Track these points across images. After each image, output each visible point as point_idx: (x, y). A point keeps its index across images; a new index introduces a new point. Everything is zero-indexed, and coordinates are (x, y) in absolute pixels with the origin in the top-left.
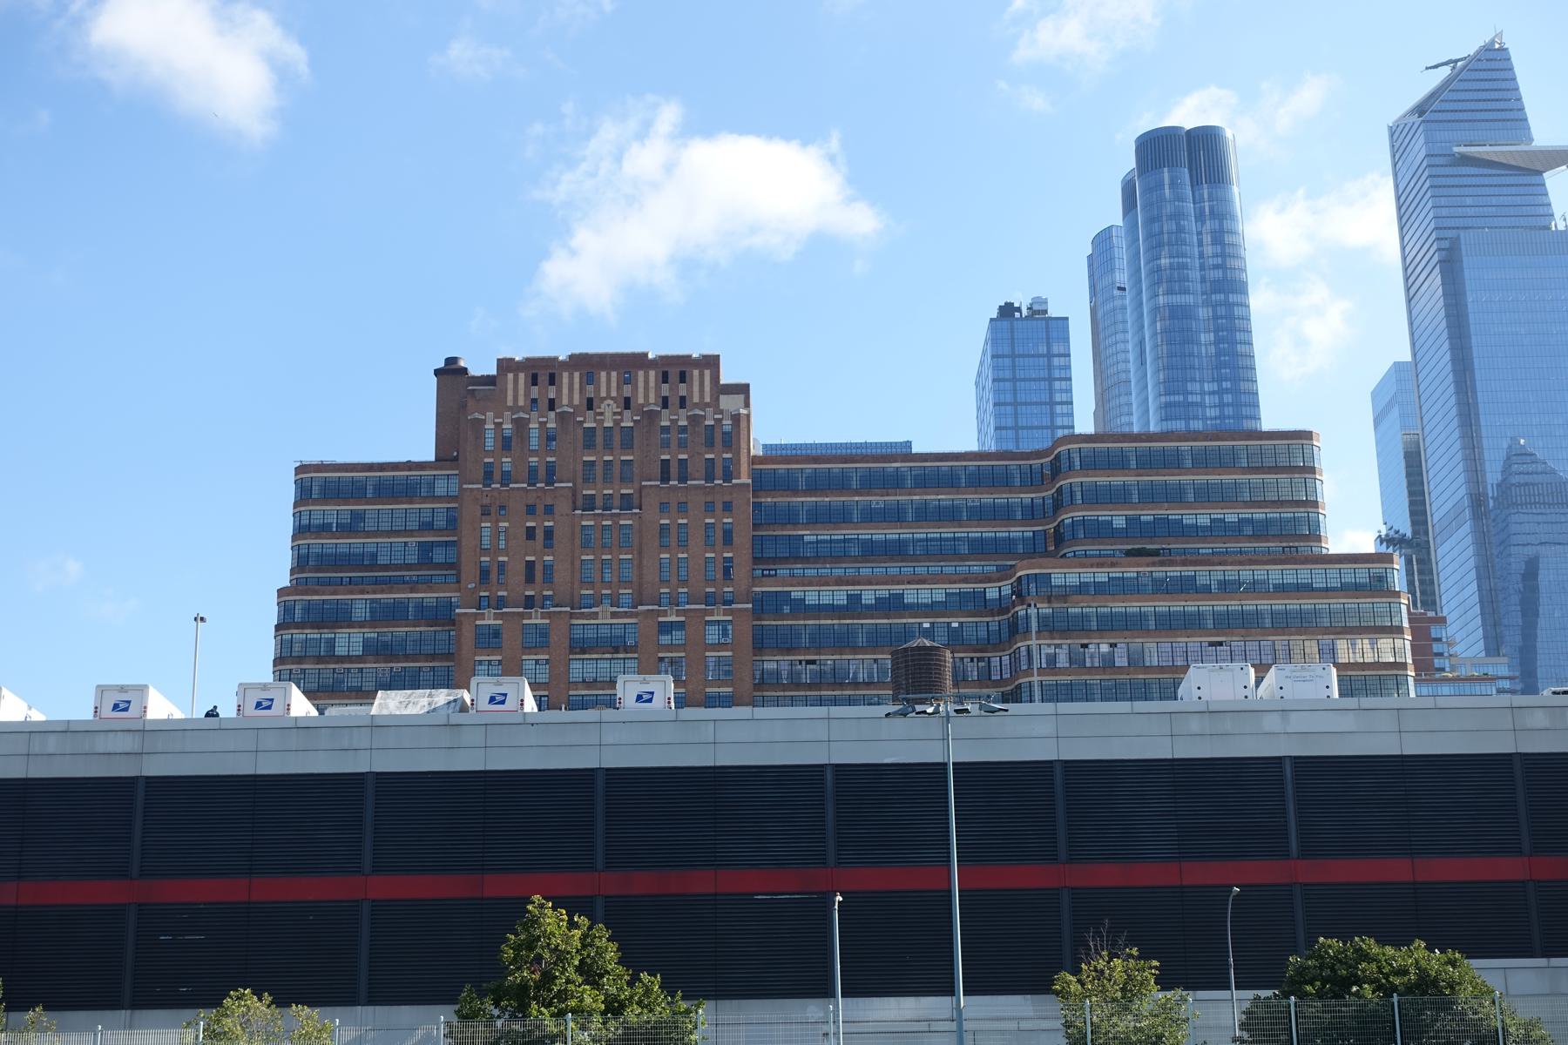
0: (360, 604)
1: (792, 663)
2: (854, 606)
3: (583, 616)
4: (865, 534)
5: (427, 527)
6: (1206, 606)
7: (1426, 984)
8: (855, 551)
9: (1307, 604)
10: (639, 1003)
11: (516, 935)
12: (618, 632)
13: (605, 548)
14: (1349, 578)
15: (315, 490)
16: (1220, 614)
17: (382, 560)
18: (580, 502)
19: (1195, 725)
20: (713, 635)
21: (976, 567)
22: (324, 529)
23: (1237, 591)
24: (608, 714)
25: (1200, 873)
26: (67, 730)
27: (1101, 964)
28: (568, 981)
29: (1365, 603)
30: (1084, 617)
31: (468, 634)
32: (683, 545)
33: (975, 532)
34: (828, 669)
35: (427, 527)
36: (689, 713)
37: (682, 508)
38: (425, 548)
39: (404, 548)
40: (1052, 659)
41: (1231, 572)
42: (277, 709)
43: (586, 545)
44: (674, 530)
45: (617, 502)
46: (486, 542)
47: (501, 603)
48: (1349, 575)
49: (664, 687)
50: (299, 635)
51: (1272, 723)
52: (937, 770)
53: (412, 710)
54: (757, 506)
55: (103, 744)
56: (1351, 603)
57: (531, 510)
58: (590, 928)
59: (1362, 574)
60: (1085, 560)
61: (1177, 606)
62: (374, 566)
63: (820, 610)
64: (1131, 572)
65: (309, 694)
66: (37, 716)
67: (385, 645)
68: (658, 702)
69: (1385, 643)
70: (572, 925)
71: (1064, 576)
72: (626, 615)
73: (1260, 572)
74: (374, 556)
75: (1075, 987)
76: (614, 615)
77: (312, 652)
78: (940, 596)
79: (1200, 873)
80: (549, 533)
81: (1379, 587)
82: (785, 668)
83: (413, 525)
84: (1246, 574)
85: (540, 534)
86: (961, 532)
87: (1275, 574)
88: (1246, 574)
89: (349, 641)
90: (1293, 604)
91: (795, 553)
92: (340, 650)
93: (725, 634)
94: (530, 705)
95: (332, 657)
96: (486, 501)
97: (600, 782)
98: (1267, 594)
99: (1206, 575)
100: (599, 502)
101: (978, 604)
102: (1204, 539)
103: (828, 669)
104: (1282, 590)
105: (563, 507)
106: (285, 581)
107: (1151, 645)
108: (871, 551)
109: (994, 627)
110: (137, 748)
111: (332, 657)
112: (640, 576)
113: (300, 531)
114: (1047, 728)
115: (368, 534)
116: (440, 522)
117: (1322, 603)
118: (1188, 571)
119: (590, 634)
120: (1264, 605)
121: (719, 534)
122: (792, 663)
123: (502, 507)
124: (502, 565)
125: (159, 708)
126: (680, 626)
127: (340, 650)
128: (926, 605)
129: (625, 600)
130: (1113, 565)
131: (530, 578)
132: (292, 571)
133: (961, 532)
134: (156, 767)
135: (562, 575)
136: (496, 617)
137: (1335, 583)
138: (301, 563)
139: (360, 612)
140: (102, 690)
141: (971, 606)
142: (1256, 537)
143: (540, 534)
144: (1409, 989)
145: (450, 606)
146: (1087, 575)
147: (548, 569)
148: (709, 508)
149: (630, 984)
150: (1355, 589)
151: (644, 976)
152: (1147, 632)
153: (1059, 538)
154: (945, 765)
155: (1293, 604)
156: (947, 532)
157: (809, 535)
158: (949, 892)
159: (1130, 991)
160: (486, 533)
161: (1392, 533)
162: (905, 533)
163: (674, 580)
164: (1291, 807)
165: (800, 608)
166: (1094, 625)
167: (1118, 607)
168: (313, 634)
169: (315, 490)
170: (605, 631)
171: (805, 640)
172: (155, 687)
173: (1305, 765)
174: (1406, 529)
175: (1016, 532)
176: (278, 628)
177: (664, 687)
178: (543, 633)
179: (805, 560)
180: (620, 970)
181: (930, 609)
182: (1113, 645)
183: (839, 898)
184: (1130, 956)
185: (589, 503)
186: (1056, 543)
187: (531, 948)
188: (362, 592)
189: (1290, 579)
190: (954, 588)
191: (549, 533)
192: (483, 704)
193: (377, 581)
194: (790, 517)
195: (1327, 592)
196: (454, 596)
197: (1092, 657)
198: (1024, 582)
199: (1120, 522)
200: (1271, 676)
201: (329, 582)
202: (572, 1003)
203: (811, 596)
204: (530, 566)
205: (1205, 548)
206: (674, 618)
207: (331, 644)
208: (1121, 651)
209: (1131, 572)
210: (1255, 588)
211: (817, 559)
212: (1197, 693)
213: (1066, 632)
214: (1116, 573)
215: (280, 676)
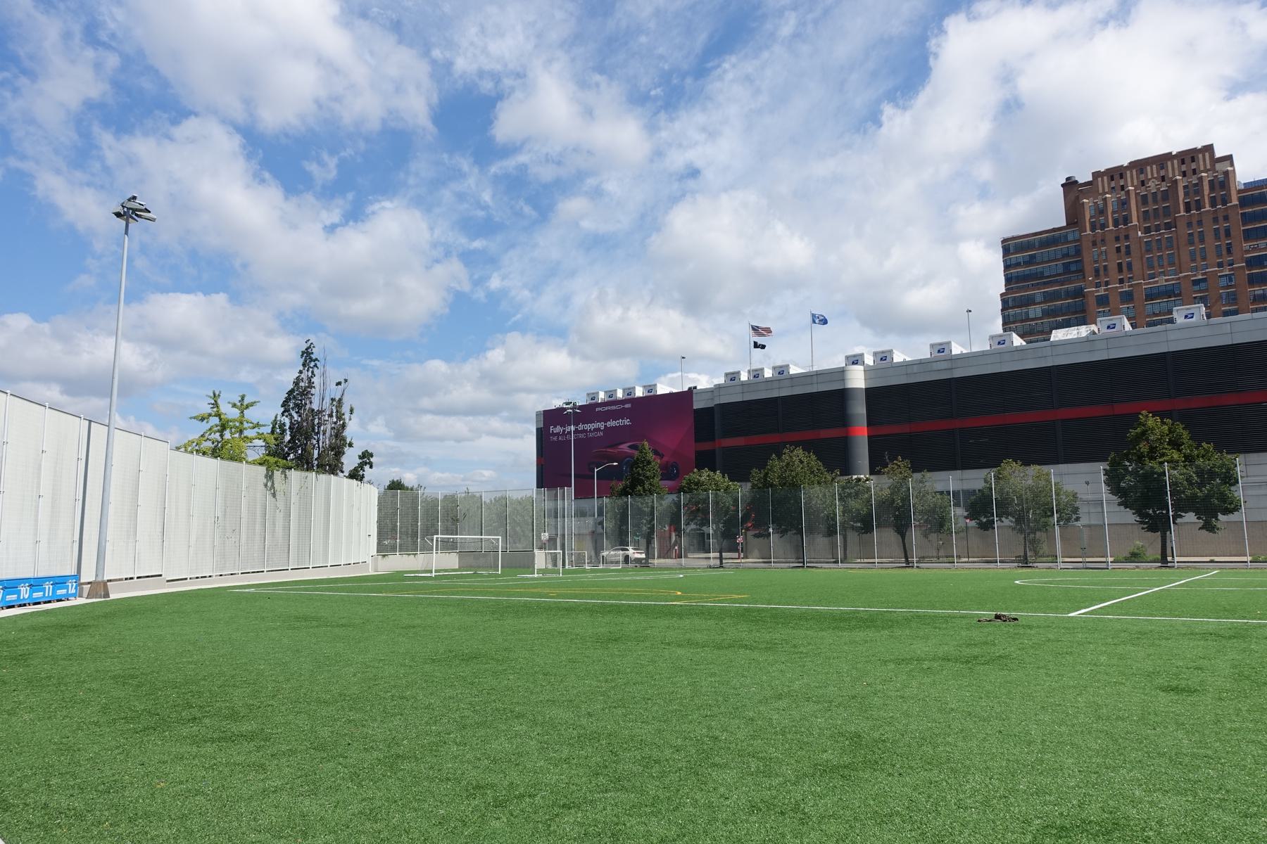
0: (1038, 293)
17: (1046, 274)
22: (1018, 265)
26: (921, 363)
31: (1092, 302)
35: (1066, 255)
38: (1066, 266)
39: (1057, 266)
50: (1011, 312)
53: (1070, 337)
70: (1163, 423)
77: (1020, 318)
80: (1128, 247)
89: (1035, 311)
92: (1031, 316)
94: (1128, 327)
110: (950, 366)
115: (1038, 264)
127: (1031, 316)
132: (1006, 286)
138: (1008, 280)
145: (1081, 289)
151: (1204, 444)
168: (1018, 310)
176: (1002, 310)
192: (1104, 330)
206: (1200, 277)
207: (1027, 313)
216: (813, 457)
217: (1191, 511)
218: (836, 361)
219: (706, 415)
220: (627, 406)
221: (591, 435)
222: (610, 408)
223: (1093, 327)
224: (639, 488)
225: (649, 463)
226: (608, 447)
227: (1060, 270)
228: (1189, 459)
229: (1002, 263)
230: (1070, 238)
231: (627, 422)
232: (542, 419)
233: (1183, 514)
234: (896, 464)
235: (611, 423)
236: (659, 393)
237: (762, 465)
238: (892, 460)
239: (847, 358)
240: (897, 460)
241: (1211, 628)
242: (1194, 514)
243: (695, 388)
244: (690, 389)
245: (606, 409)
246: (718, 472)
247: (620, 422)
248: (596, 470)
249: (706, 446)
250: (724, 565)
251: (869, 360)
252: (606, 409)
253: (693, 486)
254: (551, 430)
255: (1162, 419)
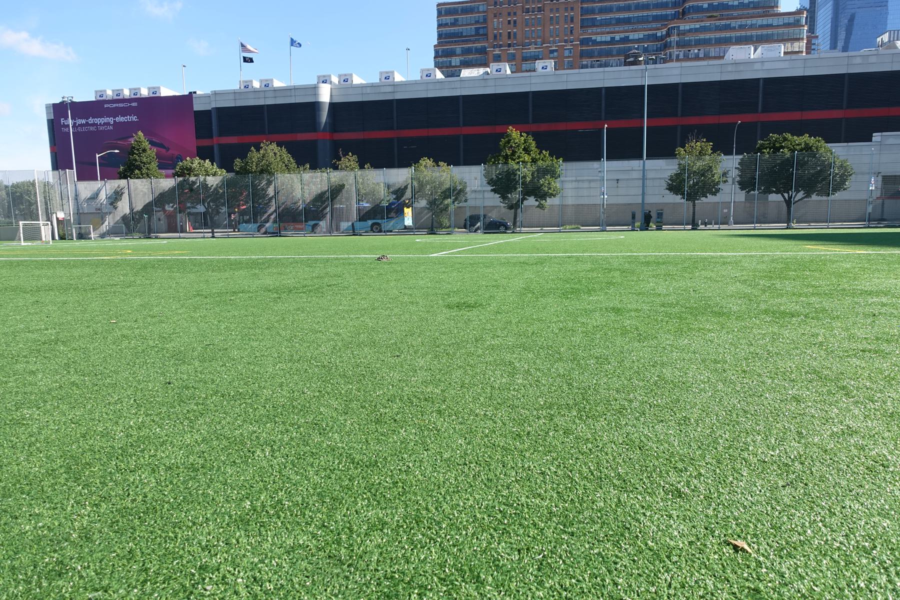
0: (458, 48)
1: (592, 61)
2: (613, 41)
3: (526, 49)
4: (617, 16)
5: (477, 22)
6: (733, 34)
7: (808, 148)
8: (614, 22)
9: (770, 31)
10: (542, 160)
11: (504, 139)
12: (537, 54)
13: (533, 26)
14: (786, 21)
15: (443, 12)
16: (738, 37)
17: (464, 34)
18: (525, 10)
19: (730, 68)
20: (567, 53)
21: (654, 25)
22: (446, 25)
23: (745, 28)
24: (533, 74)
25: (725, 119)
26: (372, 86)
27: (693, 144)
28: (521, 153)
29: (791, 30)
30: (690, 41)
31: (491, 57)
32: (558, 23)
33: (655, 13)
34: (603, 63)
35: (477, 22)
36: (558, 72)
37: (558, 10)
38: (477, 29)
39: (470, 30)
40: (678, 56)
41: (743, 22)
42: (432, 77)
43: (527, 26)
44: (555, 18)
45: (536, 9)
46: (495, 25)
47: (501, 46)
48: (787, 20)
49: (551, 64)
50: (441, 60)
51: (757, 66)
52: (642, 87)
53: (472, 75)
54: (582, 8)
55: (383, 90)
56: (786, 30)
57: (509, 14)
58: (527, 137)
59: (791, 19)
60: (693, 21)
61: (723, 35)
62: (462, 37)
63: (601, 43)
64: (708, 24)
65: (442, 72)
66: (364, 82)
67: (466, 62)
68: (549, 69)
69: (796, 44)
70: (521, 136)
71: (684, 26)
72: (539, 48)
73: (754, 21)
74: (462, 33)
75: (683, 152)
76: (536, 48)
77: (445, 65)
78: (641, 36)
79: (725, 119)
80: (515, 22)
81: (797, 24)
82: (589, 63)
83: (473, 22)
84: (749, 22)
85: (512, 22)
86: (650, 13)
87: (760, 21)
88: (749, 22)
89: (456, 61)
90: (765, 32)
91: (594, 24)
92: (453, 64)
93: (571, 53)
94: (509, 72)
95: (451, 66)
96: (495, 12)
97: (531, 96)
98: (756, 29)
99: (734, 23)
100: (531, 10)
101: (655, 38)
102: (735, 10)
103: (603, 63)
104: (762, 27)
105: (519, 12)
106: (436, 43)
107: (712, 49)
108: (619, 22)
109: (659, 46)
110: (393, 91)
111: (451, 66)
112: (544, 35)
113: (439, 26)
114: (677, 72)
115: (460, 26)
116: (481, 21)
117: (775, 31)
118: (728, 22)
119: (528, 55)
120: (754, 33)
121: (569, 19)
122: (592, 61)
123: (500, 14)
124: (501, 33)
125: (398, 78)
126: (556, 51)
127: (453, 64)
128: (636, 39)
129: (539, 43)
130: (702, 21)
131: (509, 37)
132: (438, 39)
133: (650, 13)
134: (399, 96)
135: (519, 36)
136: (499, 51)
137: (781, 23)
138: (440, 36)
139: (458, 51)
140: (381, 73)
141: (651, 39)
142: (754, 8)
143: (512, 22)
144: (801, 150)
145: (485, 48)
146: (693, 26)
147: (515, 34)
148: (566, 9)
149: (539, 154)
150: (788, 25)
151: (544, 152)
152: (711, 45)
153: (684, 13)
154: (644, 86)
155: (765, 32)
156: (645, 13)
157: (599, 17)
158: (643, 128)
159: (701, 153)
160: (495, 23)
161: (802, 8)
162: (631, 15)
163: (555, 35)
164: (761, 96)
165: (595, 43)
166: (693, 43)
167: (702, 36)
168: (445, 59)
169: (443, 12)
170: (533, 54)
171: (596, 53)
172: (398, 72)
173: (769, 81)
174: (808, 7)
175: (670, 12)
176: (435, 58)
177: (551, 64)
178: (514, 55)
179: (597, 26)
180: (536, 150)
181: (638, 41)
182: (699, 50)
183: (606, 126)
184: (703, 141)
185: (528, 11)
186: (683, 15)
187: (509, 143)
188: (459, 45)
189: (765, 23)
190: (646, 33)
191: (515, 22)
192: (494, 72)
193: (463, 41)
194: (592, 11)
195: (778, 26)
196: (486, 45)
197: (691, 54)
198: (670, 29)
199: (706, 6)
200: (759, 50)
201: (449, 42)
202: (521, 159)
203: (599, 38)
204: (509, 33)
205: (735, 13)
206: (554, 48)
207: (450, 62)
208: (702, 52)
209: (708, 24)
210: (752, 27)
211: (601, 25)
212: (731, 57)
213: (683, 46)
214: (702, 24)
215: (435, 67)
216: (284, 150)
217: (533, 195)
218: (310, 80)
219: (203, 117)
220: (134, 104)
221: (101, 128)
222: (117, 105)
223: (488, 70)
224: (137, 171)
225: (144, 150)
226: (119, 139)
227: (473, 33)
228: (534, 161)
229: (436, 22)
230: (481, 10)
231: (134, 118)
232: (52, 111)
233: (528, 198)
234: (348, 159)
235: (120, 119)
236: (162, 95)
237: (243, 156)
238: (344, 155)
239: (319, 77)
240: (348, 155)
241: (522, 260)
242: (533, 197)
243: (195, 93)
244: (190, 93)
245: (114, 105)
246: (207, 161)
247: (128, 118)
248: (97, 156)
249: (206, 142)
250: (215, 234)
251: (335, 80)
252: (114, 105)
253: (186, 172)
254: (62, 122)
255: (521, 133)
